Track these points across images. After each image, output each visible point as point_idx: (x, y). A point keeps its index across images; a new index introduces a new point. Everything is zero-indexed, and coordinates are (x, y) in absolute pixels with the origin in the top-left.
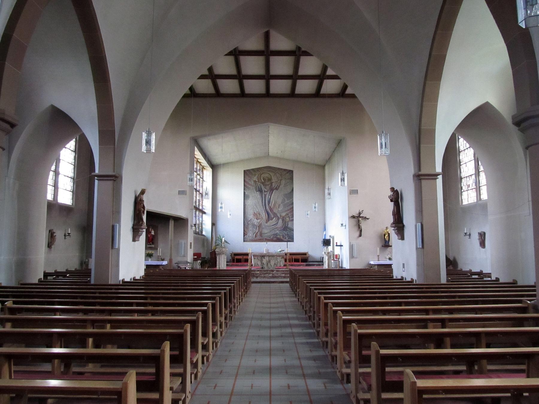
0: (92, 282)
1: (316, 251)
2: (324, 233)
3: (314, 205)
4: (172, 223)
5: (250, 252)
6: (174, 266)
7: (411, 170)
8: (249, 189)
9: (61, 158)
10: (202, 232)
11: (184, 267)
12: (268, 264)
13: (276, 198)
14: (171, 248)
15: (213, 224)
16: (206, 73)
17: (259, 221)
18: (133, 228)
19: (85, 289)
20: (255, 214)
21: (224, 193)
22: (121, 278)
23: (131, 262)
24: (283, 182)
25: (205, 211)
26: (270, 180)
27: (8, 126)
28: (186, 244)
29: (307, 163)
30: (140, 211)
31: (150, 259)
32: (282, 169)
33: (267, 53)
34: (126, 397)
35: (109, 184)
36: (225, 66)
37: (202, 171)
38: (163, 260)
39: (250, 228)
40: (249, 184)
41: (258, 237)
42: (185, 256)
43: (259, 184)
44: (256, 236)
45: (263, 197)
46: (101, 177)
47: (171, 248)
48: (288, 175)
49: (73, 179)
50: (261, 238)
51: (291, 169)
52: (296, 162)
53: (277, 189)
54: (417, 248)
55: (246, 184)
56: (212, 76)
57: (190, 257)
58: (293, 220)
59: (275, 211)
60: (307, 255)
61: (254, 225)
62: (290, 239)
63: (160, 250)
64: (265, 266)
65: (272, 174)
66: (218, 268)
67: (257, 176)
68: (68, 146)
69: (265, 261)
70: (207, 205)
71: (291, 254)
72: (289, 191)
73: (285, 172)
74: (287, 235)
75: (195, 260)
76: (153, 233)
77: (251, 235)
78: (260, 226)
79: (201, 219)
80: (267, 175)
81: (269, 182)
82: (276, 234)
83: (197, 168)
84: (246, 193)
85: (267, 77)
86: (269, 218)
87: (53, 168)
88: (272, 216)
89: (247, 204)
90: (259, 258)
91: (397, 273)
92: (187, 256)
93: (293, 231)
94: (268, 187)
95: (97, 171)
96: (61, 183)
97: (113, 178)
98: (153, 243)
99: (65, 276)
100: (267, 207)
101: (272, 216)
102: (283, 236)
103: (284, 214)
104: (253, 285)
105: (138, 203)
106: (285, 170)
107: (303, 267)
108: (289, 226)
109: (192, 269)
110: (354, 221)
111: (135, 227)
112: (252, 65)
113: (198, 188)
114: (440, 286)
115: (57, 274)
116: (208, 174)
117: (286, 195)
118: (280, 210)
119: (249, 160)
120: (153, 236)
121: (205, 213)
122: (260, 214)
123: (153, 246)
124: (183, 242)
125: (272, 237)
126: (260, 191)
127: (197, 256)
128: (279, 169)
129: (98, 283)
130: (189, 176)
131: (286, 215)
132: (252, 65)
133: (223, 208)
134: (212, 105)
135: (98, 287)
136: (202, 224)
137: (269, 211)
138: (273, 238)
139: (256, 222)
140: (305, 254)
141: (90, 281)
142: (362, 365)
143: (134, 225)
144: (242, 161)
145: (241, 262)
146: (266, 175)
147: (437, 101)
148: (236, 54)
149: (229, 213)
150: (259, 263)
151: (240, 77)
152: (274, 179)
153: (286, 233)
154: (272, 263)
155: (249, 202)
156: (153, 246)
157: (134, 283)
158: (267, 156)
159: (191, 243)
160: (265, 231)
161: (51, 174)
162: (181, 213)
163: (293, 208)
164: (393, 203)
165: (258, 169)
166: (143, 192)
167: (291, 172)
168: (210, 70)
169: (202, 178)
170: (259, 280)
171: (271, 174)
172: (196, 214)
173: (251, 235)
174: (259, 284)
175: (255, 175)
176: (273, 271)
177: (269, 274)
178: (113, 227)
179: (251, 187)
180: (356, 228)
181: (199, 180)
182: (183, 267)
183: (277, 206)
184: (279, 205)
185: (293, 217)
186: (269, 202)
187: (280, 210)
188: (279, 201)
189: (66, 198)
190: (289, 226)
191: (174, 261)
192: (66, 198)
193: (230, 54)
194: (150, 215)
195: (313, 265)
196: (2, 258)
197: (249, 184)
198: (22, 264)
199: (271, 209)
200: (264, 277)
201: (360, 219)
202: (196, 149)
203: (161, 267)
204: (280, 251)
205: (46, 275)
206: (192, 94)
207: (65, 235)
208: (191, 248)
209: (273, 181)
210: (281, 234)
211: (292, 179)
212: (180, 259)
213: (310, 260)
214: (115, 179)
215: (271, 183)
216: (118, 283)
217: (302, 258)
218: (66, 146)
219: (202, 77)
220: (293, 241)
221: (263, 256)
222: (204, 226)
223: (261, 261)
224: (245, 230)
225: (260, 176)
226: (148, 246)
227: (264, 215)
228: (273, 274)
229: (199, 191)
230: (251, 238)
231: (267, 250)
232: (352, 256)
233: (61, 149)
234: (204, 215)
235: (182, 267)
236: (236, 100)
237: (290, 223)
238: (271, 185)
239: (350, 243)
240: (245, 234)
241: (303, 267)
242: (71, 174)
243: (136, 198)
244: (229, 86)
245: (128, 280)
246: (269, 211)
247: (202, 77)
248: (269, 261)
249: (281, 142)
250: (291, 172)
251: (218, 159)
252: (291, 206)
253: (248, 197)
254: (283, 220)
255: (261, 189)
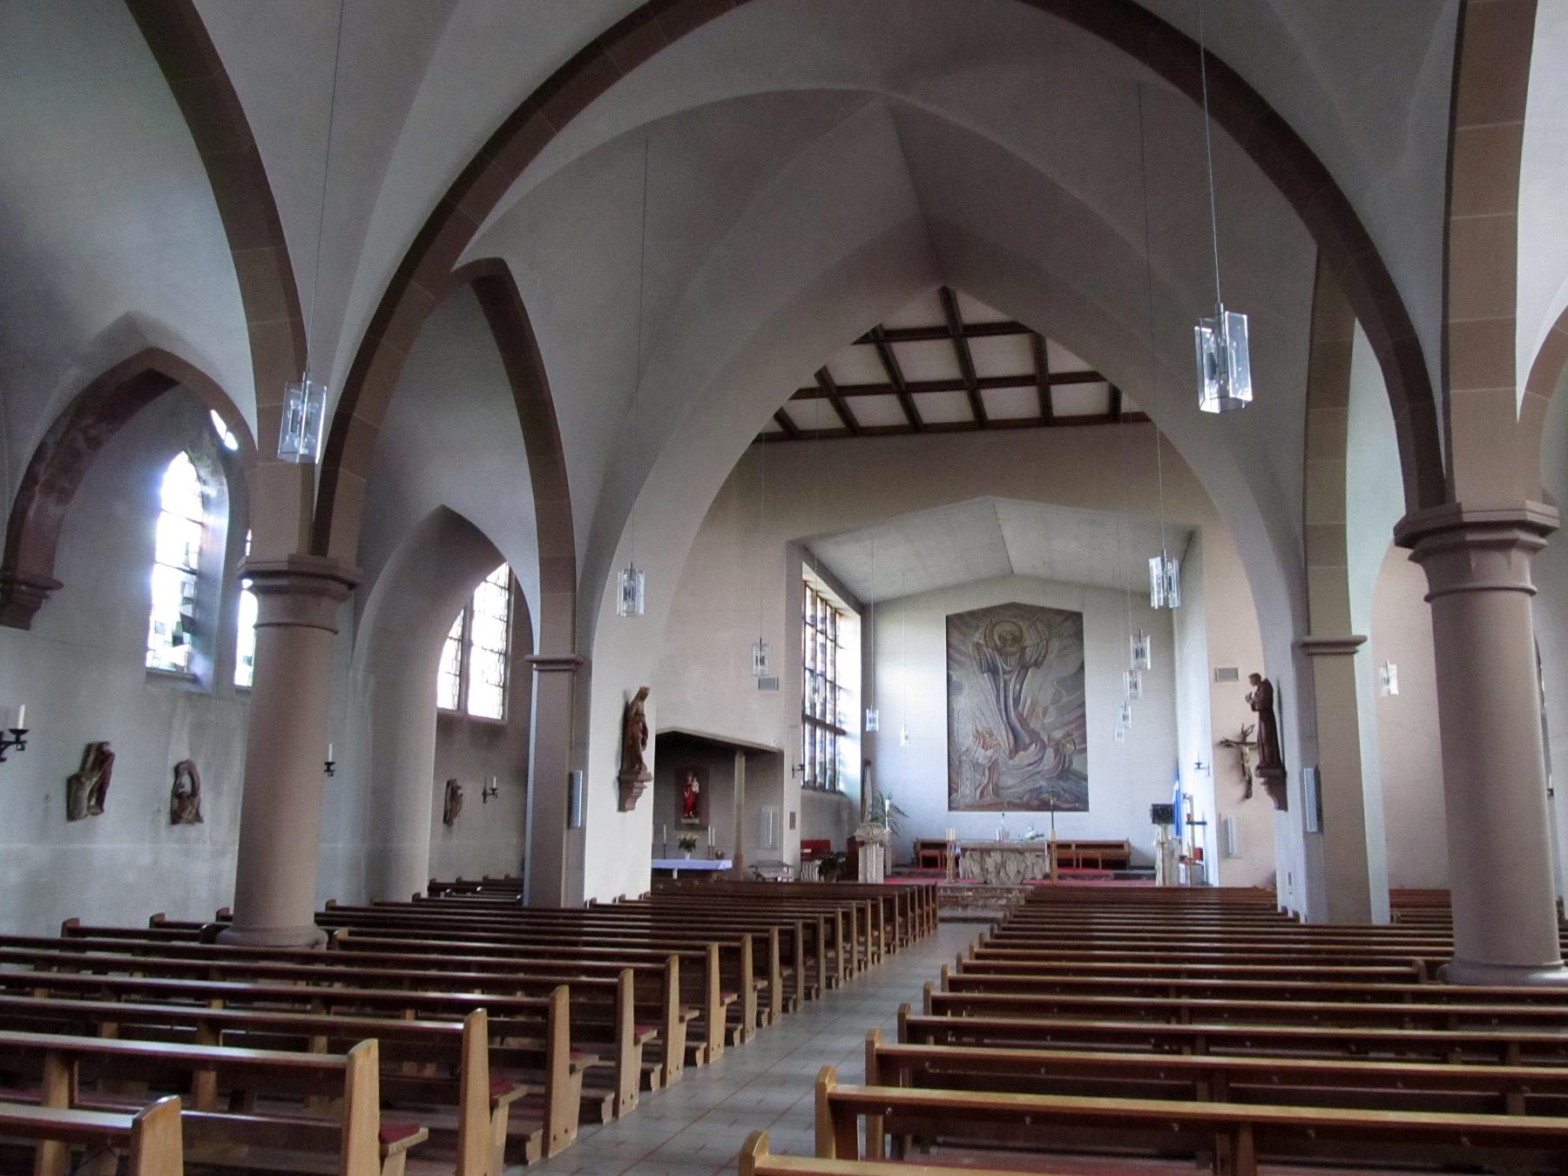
0: (526, 904)
1: (1146, 839)
2: (1176, 787)
4: (740, 763)
6: (747, 871)
7: (1286, 634)
9: (475, 607)
10: (834, 781)
11: (772, 875)
13: (1037, 689)
14: (739, 825)
15: (867, 763)
16: (814, 384)
17: (989, 752)
18: (619, 779)
19: (522, 927)
20: (978, 735)
21: (890, 677)
22: (587, 897)
23: (617, 856)
24: (1055, 645)
25: (844, 727)
26: (1017, 639)
27: (343, 588)
28: (778, 818)
30: (634, 738)
31: (688, 856)
32: (1050, 610)
33: (957, 332)
34: (468, 1042)
35: (562, 680)
36: (858, 367)
37: (834, 622)
38: (720, 857)
39: (967, 772)
40: (960, 652)
41: (989, 798)
42: (776, 846)
43: (988, 651)
45: (1000, 690)
46: (546, 665)
47: (739, 825)
48: (1068, 626)
49: (505, 655)
52: (1088, 588)
53: (1037, 664)
54: (1306, 834)
56: (826, 388)
57: (790, 850)
58: (1085, 750)
60: (1126, 849)
61: (976, 765)
62: (1079, 802)
63: (712, 831)
64: (992, 878)
65: (1024, 625)
66: (861, 879)
68: (492, 577)
69: (991, 862)
70: (848, 710)
72: (1072, 669)
73: (1060, 619)
75: (805, 858)
76: (696, 788)
77: (968, 792)
78: (993, 767)
79: (829, 749)
81: (1019, 645)
82: (1039, 790)
83: (814, 617)
84: (954, 678)
85: (971, 384)
86: (1017, 746)
87: (456, 630)
88: (1027, 740)
90: (977, 856)
91: (1281, 901)
92: (783, 845)
93: (1086, 779)
94: (1013, 660)
95: (536, 652)
96: (471, 666)
97: (572, 666)
98: (696, 815)
99: (474, 891)
100: (1013, 715)
101: (1027, 740)
103: (1058, 734)
104: (941, 926)
105: (632, 721)
106: (1059, 612)
107: (1107, 881)
109: (798, 882)
110: (1228, 755)
111: (624, 777)
112: (926, 361)
113: (819, 669)
114: (1370, 931)
115: (461, 887)
116: (850, 628)
117: (1062, 682)
118: (1049, 723)
119: (959, 588)
120: (697, 796)
121: (843, 733)
122: (991, 735)
123: (697, 821)
124: (770, 811)
126: (993, 671)
127: (813, 848)
128: (1043, 609)
129: (537, 906)
130: (756, 652)
131: (1064, 737)
132: (926, 361)
133: (888, 715)
134: (828, 460)
135: (534, 912)
136: (833, 761)
137: (1018, 726)
139: (981, 755)
140: (1120, 846)
141: (520, 901)
142: (1263, 1157)
143: (621, 772)
144: (942, 591)
145: (1096, 867)
146: (1006, 628)
147: (1344, 458)
148: (881, 340)
149: (903, 734)
150: (976, 869)
151: (902, 389)
152: (1030, 640)
153: (1066, 786)
154: (1012, 868)
155: (963, 702)
156: (697, 821)
157: (622, 908)
158: (1008, 575)
159: (793, 816)
160: (1008, 781)
161: (450, 650)
162: (765, 735)
163: (1083, 716)
164: (1257, 714)
166: (642, 695)
167: (1076, 617)
168: (822, 375)
169: (834, 641)
170: (970, 913)
172: (813, 736)
173: (968, 792)
175: (977, 628)
176: (1009, 891)
177: (999, 898)
178: (571, 778)
180: (1235, 776)
181: (824, 646)
182: (768, 875)
184: (1046, 710)
185: (1084, 740)
186: (1017, 701)
187: (1049, 723)
188: (1046, 697)
189: (487, 703)
190: (1075, 766)
191: (747, 861)
192: (487, 703)
193: (864, 340)
194: (671, 744)
195: (1138, 877)
196: (340, 845)
197: (960, 652)
198: (380, 859)
199: (1023, 721)
200: (985, 907)
201: (1246, 749)
202: (805, 567)
203: (715, 876)
205: (434, 888)
206: (787, 431)
207: (485, 794)
208: (792, 825)
209: (1028, 642)
211: (1079, 636)
212: (763, 855)
213: (1134, 861)
214: (577, 668)
215: (1023, 650)
216: (581, 907)
217: (1114, 857)
218: (489, 578)
219: (803, 394)
220: (1086, 809)
221: (984, 851)
222: (840, 768)
225: (992, 631)
226: (684, 821)
227: (1003, 737)
229: (823, 675)
230: (968, 801)
232: (1225, 853)
233: (478, 584)
234: (841, 740)
235: (766, 875)
236: (897, 440)
237: (1076, 759)
239: (1219, 816)
240: (951, 790)
241: (1107, 881)
242: (500, 645)
243: (627, 709)
244: (878, 411)
245: (609, 901)
246: (1018, 726)
247: (803, 394)
248: (1003, 865)
249: (1035, 541)
250: (1076, 617)
253: (960, 688)
254: (1057, 751)
255: (996, 667)
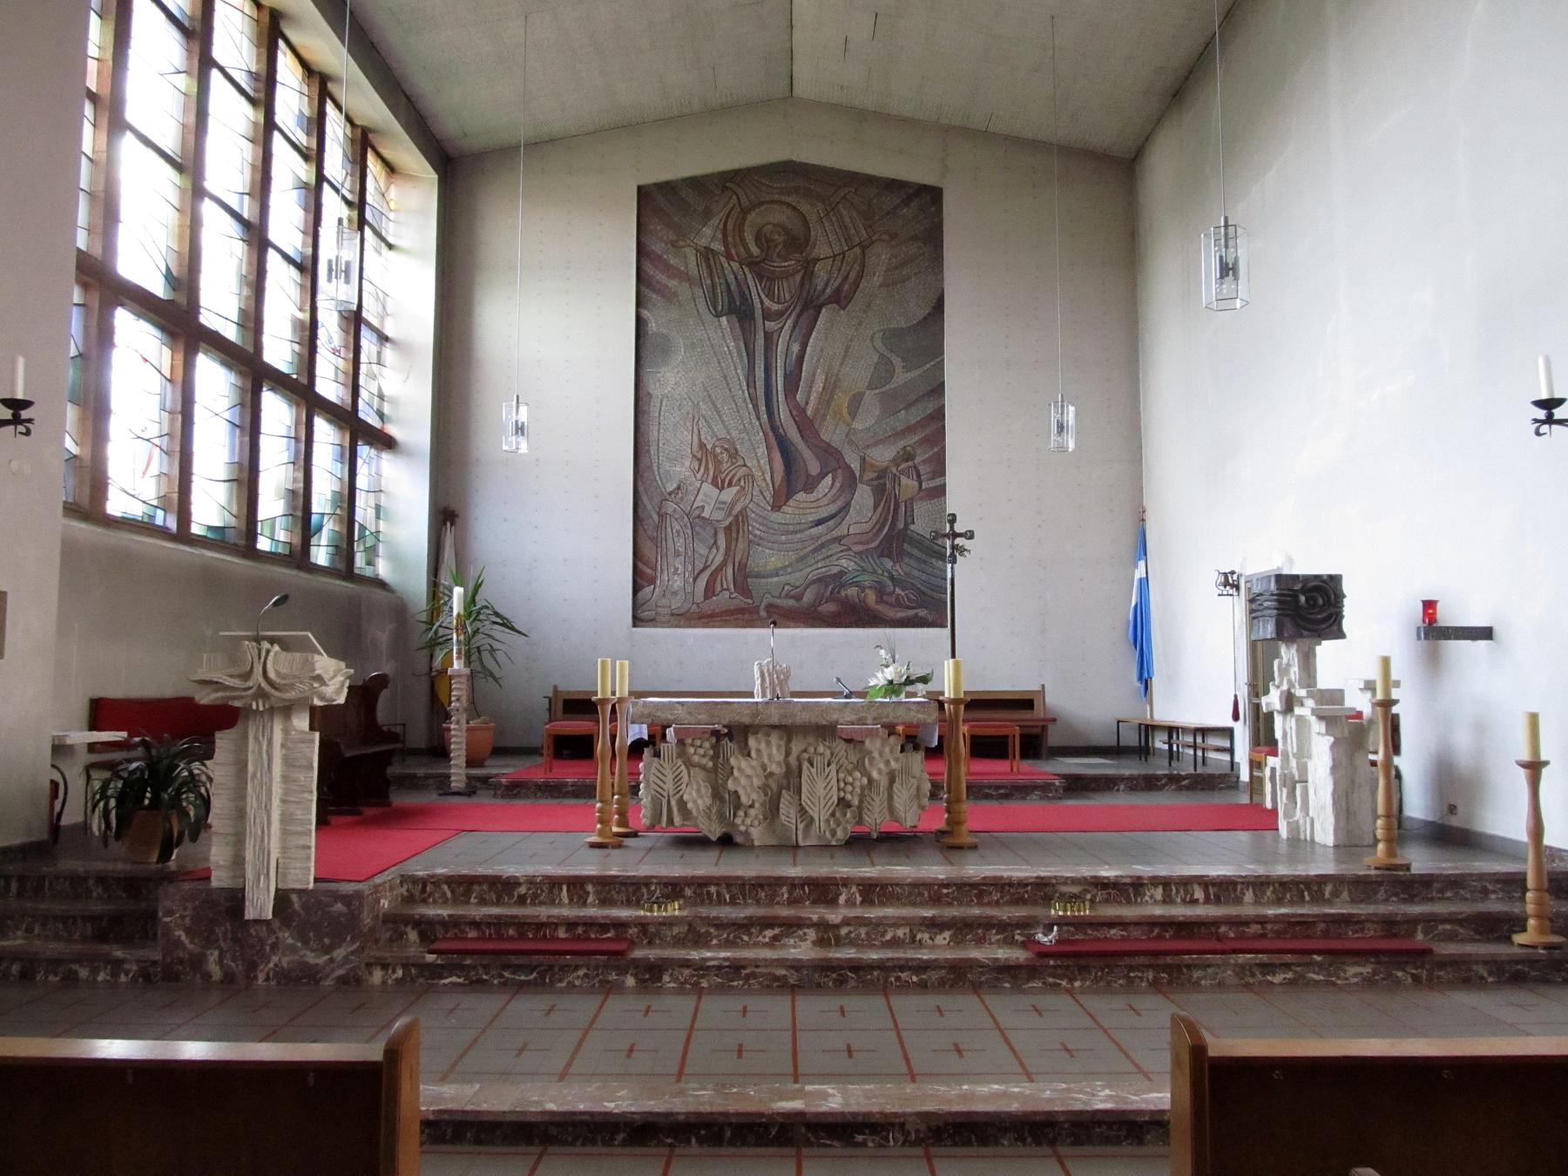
2: (1139, 573)
3: (1054, 418)
5: (623, 690)
8: (668, 296)
12: (772, 809)
13: (841, 354)
15: (447, 516)
17: (728, 494)
20: (704, 454)
24: (881, 256)
26: (797, 243)
29: (1035, 146)
32: (869, 180)
39: (676, 538)
41: (725, 598)
43: (731, 268)
44: (709, 592)
50: (741, 601)
51: (930, 179)
55: (649, 268)
59: (831, 433)
60: (1038, 712)
61: (697, 521)
62: (929, 607)
67: (715, 221)
71: (978, 704)
72: (918, 311)
74: (905, 579)
77: (678, 583)
78: (736, 526)
80: (780, 216)
84: (652, 326)
86: (792, 482)
88: (814, 468)
89: (653, 387)
94: (786, 290)
101: (814, 468)
102: (881, 592)
103: (883, 455)
106: (893, 185)
108: (921, 527)
117: (893, 338)
118: (865, 435)
122: (734, 454)
125: (808, 597)
126: (740, 311)
131: (896, 461)
137: (793, 434)
138: (819, 600)
139: (709, 499)
140: (1025, 703)
144: (626, 128)
153: (898, 570)
155: (669, 380)
158: (782, 101)
160: (768, 558)
163: (939, 415)
165: (728, 181)
167: (933, 196)
171: (805, 207)
173: (678, 583)
174: (681, 1048)
175: (707, 215)
179: (683, 290)
183: (842, 400)
187: (865, 435)
188: (857, 374)
197: (668, 269)
199: (806, 425)
204: (892, 687)
209: (822, 250)
210: (866, 579)
211: (933, 238)
215: (808, 266)
223: (718, 775)
224: (647, 549)
227: (760, 460)
228: (827, 934)
230: (676, 603)
231: (777, 678)
238: (808, 274)
240: (641, 578)
246: (793, 434)
248: (792, 779)
250: (933, 196)
251: (475, 103)
252: (930, 407)
253: (665, 349)
254: (879, 492)
